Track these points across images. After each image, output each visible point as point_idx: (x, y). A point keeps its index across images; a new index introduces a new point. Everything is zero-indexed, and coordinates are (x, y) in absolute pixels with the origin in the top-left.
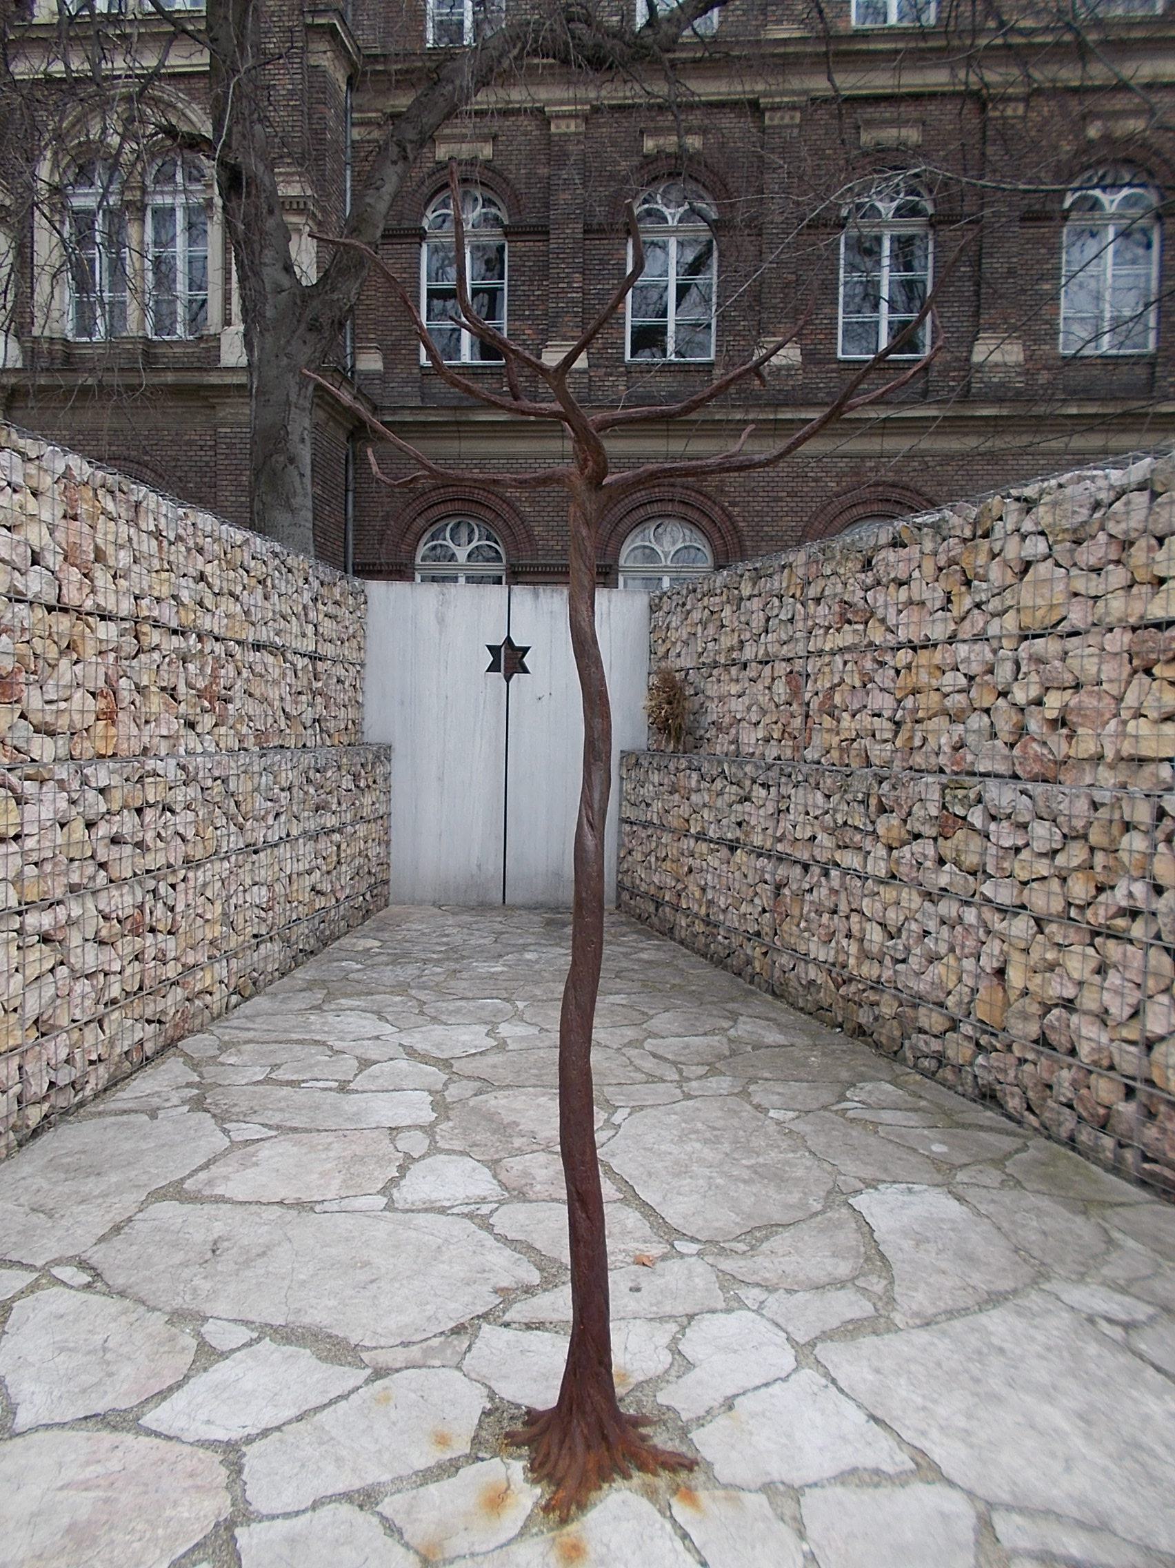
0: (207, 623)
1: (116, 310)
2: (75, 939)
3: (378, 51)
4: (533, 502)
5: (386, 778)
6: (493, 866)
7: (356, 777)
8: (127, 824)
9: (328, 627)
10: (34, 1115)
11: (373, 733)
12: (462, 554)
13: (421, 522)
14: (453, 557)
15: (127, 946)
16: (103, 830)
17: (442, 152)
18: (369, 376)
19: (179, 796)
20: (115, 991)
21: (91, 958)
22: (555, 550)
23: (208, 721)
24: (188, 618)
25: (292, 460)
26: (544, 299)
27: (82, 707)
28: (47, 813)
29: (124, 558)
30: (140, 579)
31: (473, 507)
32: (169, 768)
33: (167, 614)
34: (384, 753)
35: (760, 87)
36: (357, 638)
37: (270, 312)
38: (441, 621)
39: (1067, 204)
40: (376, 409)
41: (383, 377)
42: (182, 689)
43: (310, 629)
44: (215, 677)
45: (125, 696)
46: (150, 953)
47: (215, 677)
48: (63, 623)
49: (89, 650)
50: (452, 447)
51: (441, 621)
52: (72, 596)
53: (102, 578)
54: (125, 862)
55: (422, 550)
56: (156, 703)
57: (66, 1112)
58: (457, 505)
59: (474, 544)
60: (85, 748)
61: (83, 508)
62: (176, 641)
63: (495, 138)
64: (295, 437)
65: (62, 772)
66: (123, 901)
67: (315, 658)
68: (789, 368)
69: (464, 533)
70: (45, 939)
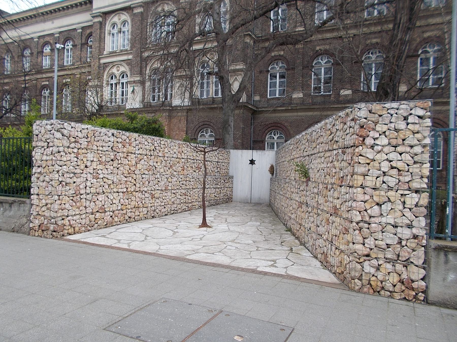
0: (198, 158)
1: (208, 92)
2: (177, 194)
3: (260, 35)
4: (290, 126)
5: (232, 181)
6: (249, 196)
7: (224, 181)
8: (184, 182)
9: (221, 157)
10: (172, 212)
11: (231, 174)
12: (276, 138)
13: (267, 131)
14: (274, 139)
15: (184, 197)
16: (181, 183)
17: (273, 54)
18: (257, 101)
19: (192, 180)
20: (182, 201)
21: (179, 197)
22: (257, 144)
23: (197, 171)
24: (194, 158)
25: (229, 125)
26: (294, 83)
27: (180, 169)
28: (175, 180)
29: (186, 152)
30: (188, 154)
31: (278, 128)
32: (191, 177)
33: (192, 158)
34: (232, 177)
35: (342, 34)
36: (228, 158)
37: (227, 100)
38: (242, 156)
39: (419, 53)
40: (257, 108)
41: (260, 101)
42: (193, 167)
43: (217, 158)
44: (199, 165)
45: (185, 168)
46: (187, 198)
47: (199, 165)
48: (178, 160)
49: (181, 163)
50: (274, 115)
51: (242, 156)
52: (179, 157)
53: (183, 154)
54: (184, 187)
55: (267, 137)
56: (189, 169)
57: (176, 213)
58: (275, 127)
59: (278, 135)
60: (180, 173)
61: (181, 147)
62: (193, 161)
63: (284, 50)
64: (230, 121)
65: (176, 176)
66: (184, 191)
67: (217, 162)
68: (348, 95)
69: (276, 132)
70: (174, 193)
